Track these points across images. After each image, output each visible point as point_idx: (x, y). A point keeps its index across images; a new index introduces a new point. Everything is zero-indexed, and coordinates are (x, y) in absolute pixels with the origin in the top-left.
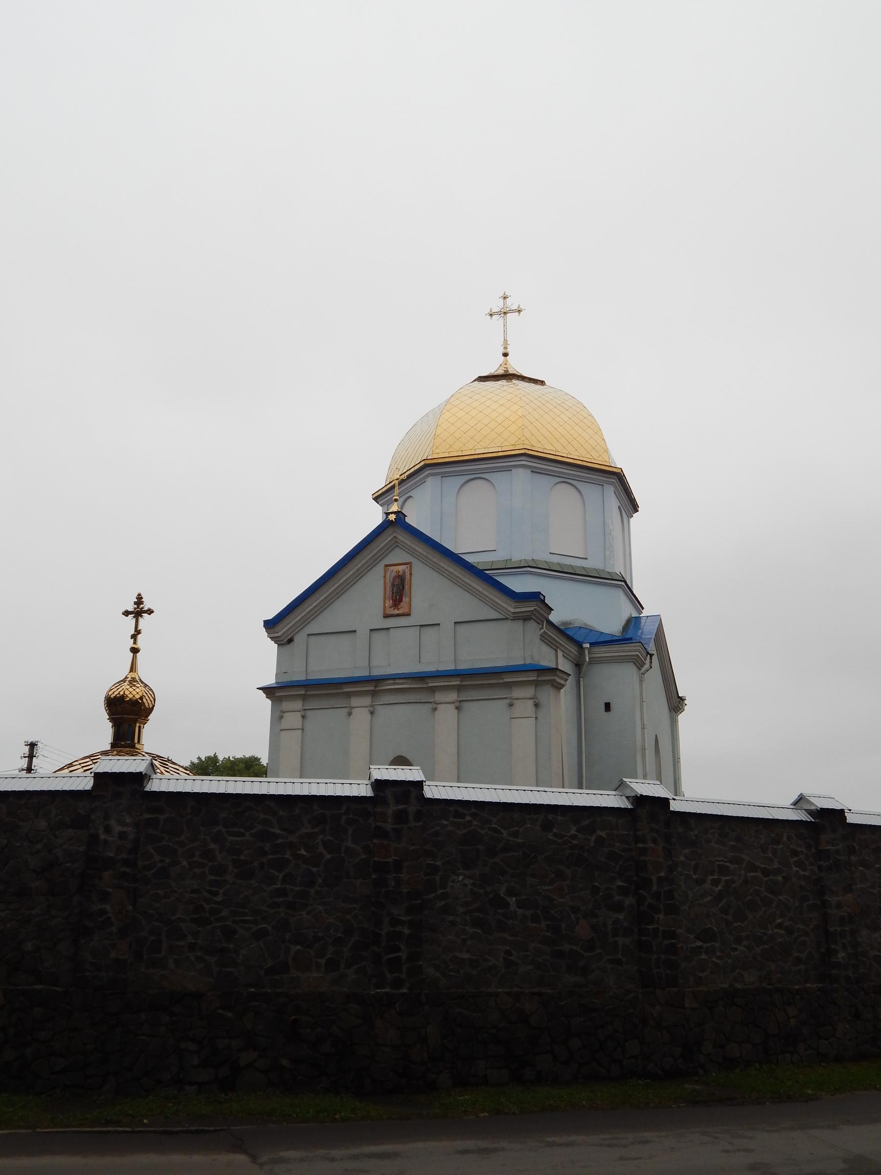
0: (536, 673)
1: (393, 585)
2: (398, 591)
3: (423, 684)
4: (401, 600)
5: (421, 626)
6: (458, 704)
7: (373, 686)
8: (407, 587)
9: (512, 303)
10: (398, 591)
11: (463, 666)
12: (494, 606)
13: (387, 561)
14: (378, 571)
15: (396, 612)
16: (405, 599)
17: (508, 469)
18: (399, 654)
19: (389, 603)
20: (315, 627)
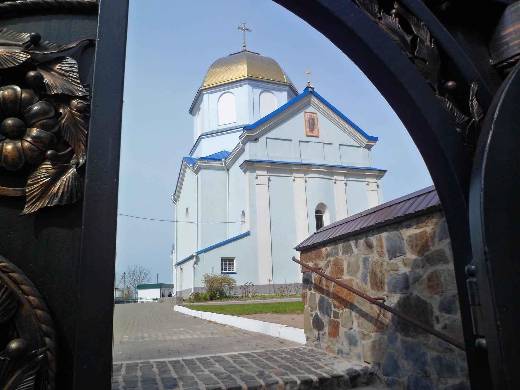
0: (378, 172)
1: (309, 121)
2: (312, 125)
3: (330, 170)
4: (313, 130)
5: (324, 143)
6: (268, 177)
7: (306, 168)
8: (316, 124)
9: (247, 26)
10: (312, 125)
11: (271, 159)
12: (356, 139)
13: (306, 111)
14: (302, 115)
15: (312, 134)
16: (316, 130)
17: (242, 85)
18: (311, 155)
19: (308, 130)
20: (269, 135)
